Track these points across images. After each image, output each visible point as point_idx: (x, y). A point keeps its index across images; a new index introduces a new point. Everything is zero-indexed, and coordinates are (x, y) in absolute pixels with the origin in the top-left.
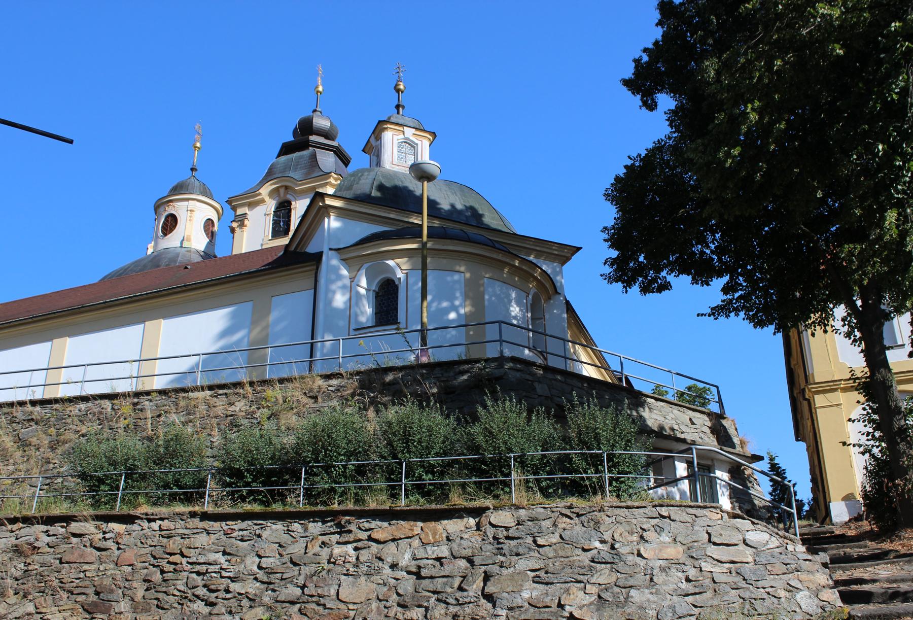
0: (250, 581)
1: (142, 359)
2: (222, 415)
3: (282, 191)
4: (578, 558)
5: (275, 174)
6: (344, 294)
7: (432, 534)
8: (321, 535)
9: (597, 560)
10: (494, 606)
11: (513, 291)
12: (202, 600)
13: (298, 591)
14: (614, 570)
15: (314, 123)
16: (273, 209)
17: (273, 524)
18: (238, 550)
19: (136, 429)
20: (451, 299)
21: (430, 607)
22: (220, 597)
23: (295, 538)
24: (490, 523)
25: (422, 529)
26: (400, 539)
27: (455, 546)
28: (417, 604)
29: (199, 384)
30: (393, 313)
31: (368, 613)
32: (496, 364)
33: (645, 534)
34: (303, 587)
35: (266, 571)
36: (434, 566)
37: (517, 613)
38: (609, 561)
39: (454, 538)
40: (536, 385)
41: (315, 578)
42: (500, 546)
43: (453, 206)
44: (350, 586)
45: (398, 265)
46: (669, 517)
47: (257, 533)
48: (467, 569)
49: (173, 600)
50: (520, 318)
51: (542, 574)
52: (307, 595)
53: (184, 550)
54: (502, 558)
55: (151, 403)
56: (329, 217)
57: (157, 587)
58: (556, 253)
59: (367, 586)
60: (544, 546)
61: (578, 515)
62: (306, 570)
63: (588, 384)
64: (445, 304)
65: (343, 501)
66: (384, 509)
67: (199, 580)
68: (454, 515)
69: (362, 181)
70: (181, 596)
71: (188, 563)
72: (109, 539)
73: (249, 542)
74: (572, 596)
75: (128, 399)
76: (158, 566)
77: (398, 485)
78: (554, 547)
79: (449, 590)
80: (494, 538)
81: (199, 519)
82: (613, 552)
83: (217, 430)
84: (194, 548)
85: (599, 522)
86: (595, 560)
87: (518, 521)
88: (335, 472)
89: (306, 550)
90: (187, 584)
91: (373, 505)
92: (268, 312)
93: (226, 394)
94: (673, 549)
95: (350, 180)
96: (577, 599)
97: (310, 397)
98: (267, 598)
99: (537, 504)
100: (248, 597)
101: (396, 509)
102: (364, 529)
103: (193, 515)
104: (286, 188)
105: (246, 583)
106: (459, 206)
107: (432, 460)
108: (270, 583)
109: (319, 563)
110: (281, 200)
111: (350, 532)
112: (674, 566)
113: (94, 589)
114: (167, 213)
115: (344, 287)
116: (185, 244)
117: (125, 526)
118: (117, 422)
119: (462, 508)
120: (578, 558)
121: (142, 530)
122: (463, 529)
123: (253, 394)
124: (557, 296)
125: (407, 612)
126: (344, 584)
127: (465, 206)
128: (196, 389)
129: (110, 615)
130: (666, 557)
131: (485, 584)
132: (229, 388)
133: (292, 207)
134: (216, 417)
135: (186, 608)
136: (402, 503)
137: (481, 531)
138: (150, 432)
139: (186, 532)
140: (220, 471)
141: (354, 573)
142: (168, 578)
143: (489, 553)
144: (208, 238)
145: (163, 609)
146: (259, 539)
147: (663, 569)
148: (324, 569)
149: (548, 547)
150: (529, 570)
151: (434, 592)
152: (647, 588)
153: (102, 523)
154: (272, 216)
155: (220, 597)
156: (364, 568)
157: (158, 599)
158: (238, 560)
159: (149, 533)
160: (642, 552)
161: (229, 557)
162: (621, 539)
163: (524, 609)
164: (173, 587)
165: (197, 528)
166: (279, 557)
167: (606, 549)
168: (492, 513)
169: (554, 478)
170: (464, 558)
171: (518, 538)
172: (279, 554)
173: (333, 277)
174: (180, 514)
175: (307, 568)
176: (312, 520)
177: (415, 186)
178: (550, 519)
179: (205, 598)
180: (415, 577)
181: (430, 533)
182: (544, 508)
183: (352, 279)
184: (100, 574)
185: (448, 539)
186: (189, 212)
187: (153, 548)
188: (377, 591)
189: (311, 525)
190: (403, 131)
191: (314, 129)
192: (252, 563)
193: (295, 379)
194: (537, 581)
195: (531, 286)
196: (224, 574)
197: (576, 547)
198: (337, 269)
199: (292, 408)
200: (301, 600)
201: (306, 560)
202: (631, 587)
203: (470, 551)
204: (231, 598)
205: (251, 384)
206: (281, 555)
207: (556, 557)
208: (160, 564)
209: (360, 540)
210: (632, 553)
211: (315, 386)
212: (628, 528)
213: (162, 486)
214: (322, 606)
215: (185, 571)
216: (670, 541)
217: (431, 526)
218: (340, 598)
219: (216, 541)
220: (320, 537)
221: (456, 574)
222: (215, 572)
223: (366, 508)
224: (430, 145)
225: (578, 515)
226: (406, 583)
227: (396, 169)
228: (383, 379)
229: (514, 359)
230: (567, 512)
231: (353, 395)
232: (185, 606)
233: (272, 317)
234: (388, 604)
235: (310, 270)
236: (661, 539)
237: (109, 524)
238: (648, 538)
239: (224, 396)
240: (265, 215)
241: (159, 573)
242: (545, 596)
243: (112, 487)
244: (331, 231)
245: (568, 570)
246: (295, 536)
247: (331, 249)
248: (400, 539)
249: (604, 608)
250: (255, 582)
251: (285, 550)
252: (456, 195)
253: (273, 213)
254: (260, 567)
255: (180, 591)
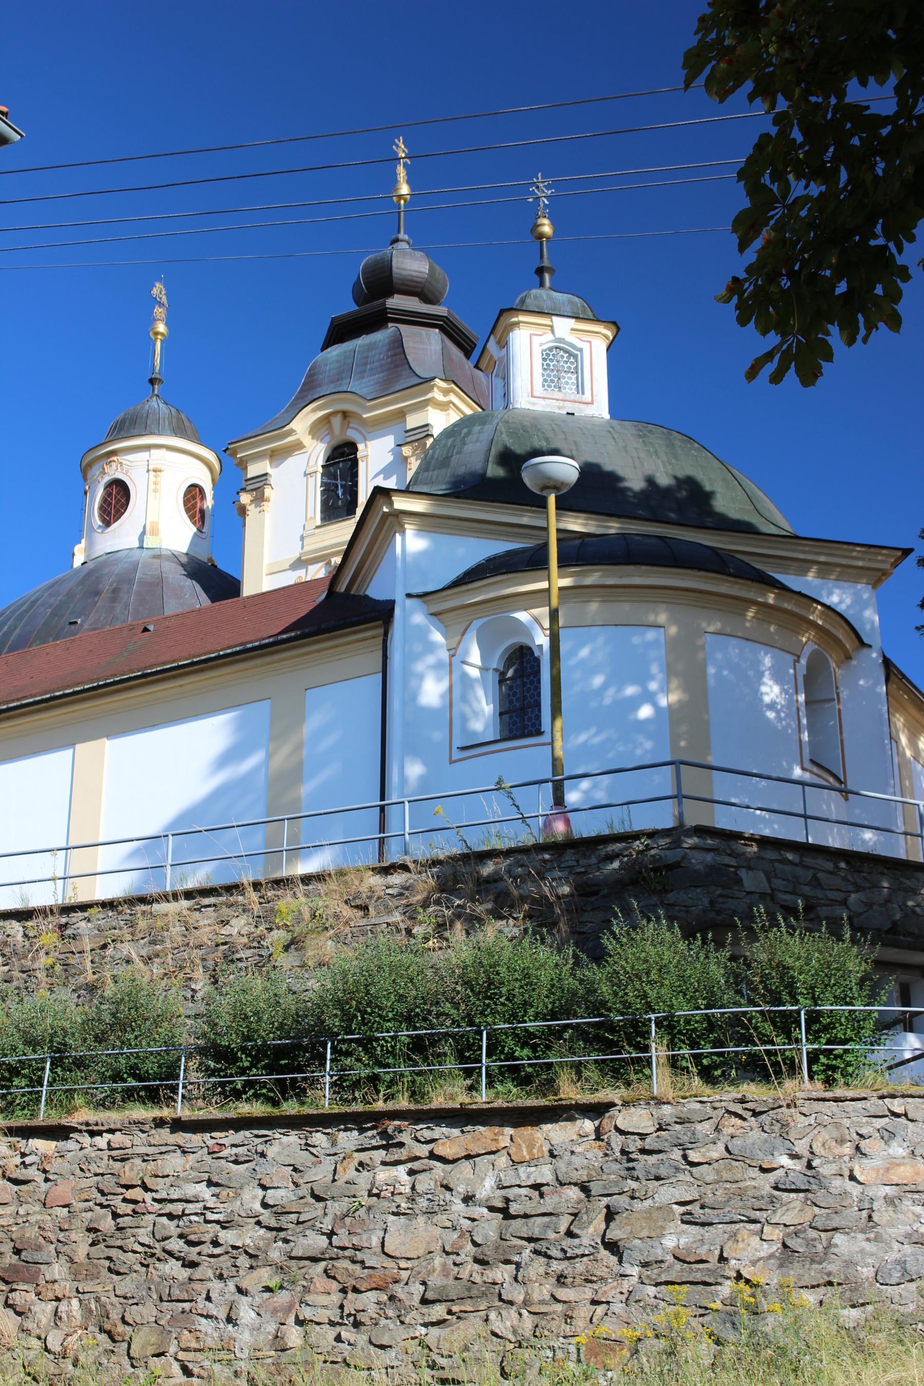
0: (250, 1226)
1: (71, 844)
2: (209, 943)
3: (337, 421)
4: (753, 1183)
5: (320, 386)
6: (439, 680)
7: (527, 1147)
8: (358, 1151)
9: (783, 1187)
10: (620, 1261)
11: (766, 654)
12: (178, 1259)
13: (323, 1241)
14: (809, 1203)
15: (395, 270)
16: (321, 461)
17: (283, 1134)
18: (230, 1179)
19: (66, 970)
20: (642, 679)
21: (523, 1264)
22: (204, 1253)
23: (317, 1157)
24: (617, 1129)
25: (512, 1139)
26: (478, 1155)
27: (561, 1165)
28: (502, 1258)
29: (168, 889)
30: (532, 712)
31: (429, 1273)
32: (668, 840)
33: (863, 1144)
34: (331, 1234)
35: (273, 1209)
36: (530, 1199)
37: (655, 1271)
38: (803, 1187)
39: (561, 1153)
40: (743, 873)
41: (348, 1220)
42: (631, 1165)
43: (650, 481)
44: (401, 1232)
45: (536, 620)
46: (906, 1115)
47: (259, 1150)
48: (579, 1202)
49: (134, 1260)
50: (783, 706)
51: (695, 1208)
52: (336, 1247)
53: (148, 1180)
54: (634, 1185)
55: (89, 925)
56: (403, 532)
57: (107, 1239)
58: (860, 563)
59: (426, 1230)
60: (699, 1164)
61: (755, 1114)
62: (335, 1208)
63: (848, 863)
64: (631, 690)
65: (393, 1095)
66: (452, 1108)
67: (171, 1227)
68: (561, 1116)
69: (469, 447)
70: (146, 1253)
71: (154, 1200)
72: (31, 1165)
73: (246, 1165)
74: (741, 1245)
75: (50, 918)
76: (108, 1206)
77: (475, 1068)
78: (715, 1165)
79: (552, 1236)
80: (623, 1152)
81: (168, 1130)
82: (809, 1173)
83: (201, 970)
84: (163, 1177)
85: (788, 1125)
86: (780, 1186)
87: (659, 1124)
88: (379, 1049)
89: (334, 1175)
90: (153, 1234)
91: (438, 1101)
92: (300, 720)
93: (215, 905)
94: (908, 1168)
95: (445, 445)
96: (749, 1248)
97: (357, 907)
98: (276, 1253)
99: (691, 1096)
100: (246, 1252)
101: (470, 1107)
102: (423, 1140)
103: (159, 1123)
104: (345, 414)
105: (244, 1229)
106: (664, 480)
107: (532, 1025)
108: (280, 1229)
109: (354, 1196)
110: (335, 442)
111: (401, 1145)
112: (909, 1195)
113: (12, 1244)
114: (107, 479)
115: (438, 666)
116: (149, 542)
117: (55, 1143)
118: (34, 959)
119: (571, 1104)
120: (753, 1183)
121: (81, 1149)
122: (575, 1137)
123: (260, 903)
124: (865, 651)
125: (487, 1272)
126: (391, 1229)
127: (676, 478)
128: (165, 897)
129: (37, 1285)
130: (896, 1180)
131: (608, 1227)
132: (220, 895)
133: (359, 455)
134: (199, 947)
135: (153, 1271)
136: (483, 1098)
137: (602, 1140)
138: (90, 977)
139: (150, 1150)
140: (202, 1051)
141: (408, 1211)
142: (124, 1225)
143: (613, 1176)
144: (194, 523)
145: (118, 1273)
146: (262, 1160)
147: (890, 1201)
148: (362, 1206)
149: (706, 1166)
150: (676, 1203)
151: (530, 1240)
152: (863, 1231)
153: (19, 1139)
154: (319, 476)
155: (204, 1253)
156: (423, 1203)
157: (109, 1258)
158: (231, 1194)
159: (93, 1155)
160: (857, 1174)
161: (216, 1190)
162: (823, 1153)
163: (667, 1264)
164: (132, 1239)
165: (166, 1145)
166: (294, 1188)
167: (798, 1168)
168: (619, 1111)
169: (724, 1052)
170: (575, 1184)
171: (660, 1152)
172: (294, 1183)
173: (418, 648)
174: (139, 1123)
175: (336, 1205)
176: (342, 1127)
177: (574, 448)
178: (711, 1120)
179: (182, 1254)
180: (501, 1216)
181: (523, 1145)
182: (701, 1102)
183: (453, 651)
184: (20, 1221)
185: (552, 1155)
186: (152, 473)
187: (99, 1178)
188: (442, 1238)
189: (342, 1135)
190: (552, 327)
191: (395, 281)
192: (252, 1199)
193: (330, 875)
194: (688, 1220)
195: (804, 640)
196: (210, 1216)
197: (750, 1166)
198: (422, 634)
199: (326, 928)
200: (327, 1256)
201: (335, 1192)
202: (835, 1229)
203: (585, 1172)
204: (222, 1254)
205: (256, 886)
206: (296, 1185)
207: (717, 1182)
208: (111, 1203)
209: (416, 1158)
210: (841, 1175)
211: (364, 888)
212: (836, 1134)
213: (110, 1077)
214: (359, 1265)
215: (149, 1213)
216: (905, 1154)
217: (525, 1133)
218: (386, 1250)
219: (196, 1165)
220: (356, 1154)
221: (562, 1210)
222: (196, 1214)
223: (425, 1107)
224: (608, 349)
225: (755, 1114)
226: (486, 1225)
227: (541, 406)
228: (478, 873)
229: (701, 831)
230: (738, 1108)
231: (425, 904)
232: (151, 1269)
233: (312, 723)
234: (458, 1260)
235: (374, 637)
236: (891, 1151)
237: (30, 1140)
238: (867, 1149)
239: (212, 909)
240: (306, 475)
241: (110, 1217)
242: (699, 1244)
243: (31, 1080)
244: (408, 559)
245: (736, 1202)
246: (317, 1154)
247: (409, 596)
248: (478, 1155)
249: (791, 1263)
250: (257, 1228)
251: (302, 1177)
252: (658, 457)
253: (320, 470)
254: (265, 1205)
255: (143, 1245)
